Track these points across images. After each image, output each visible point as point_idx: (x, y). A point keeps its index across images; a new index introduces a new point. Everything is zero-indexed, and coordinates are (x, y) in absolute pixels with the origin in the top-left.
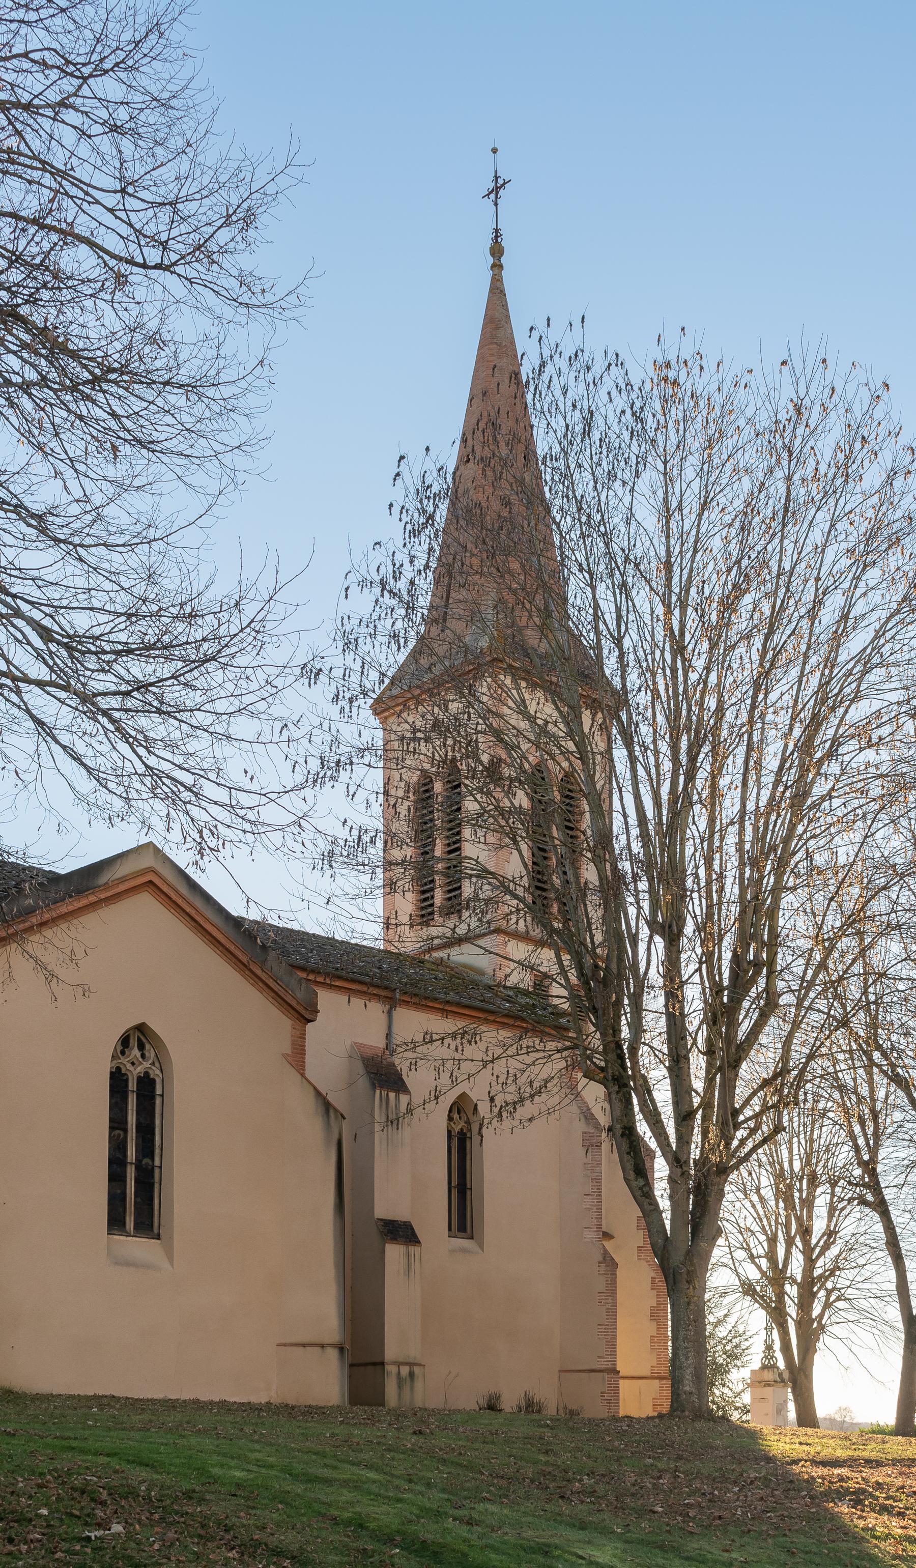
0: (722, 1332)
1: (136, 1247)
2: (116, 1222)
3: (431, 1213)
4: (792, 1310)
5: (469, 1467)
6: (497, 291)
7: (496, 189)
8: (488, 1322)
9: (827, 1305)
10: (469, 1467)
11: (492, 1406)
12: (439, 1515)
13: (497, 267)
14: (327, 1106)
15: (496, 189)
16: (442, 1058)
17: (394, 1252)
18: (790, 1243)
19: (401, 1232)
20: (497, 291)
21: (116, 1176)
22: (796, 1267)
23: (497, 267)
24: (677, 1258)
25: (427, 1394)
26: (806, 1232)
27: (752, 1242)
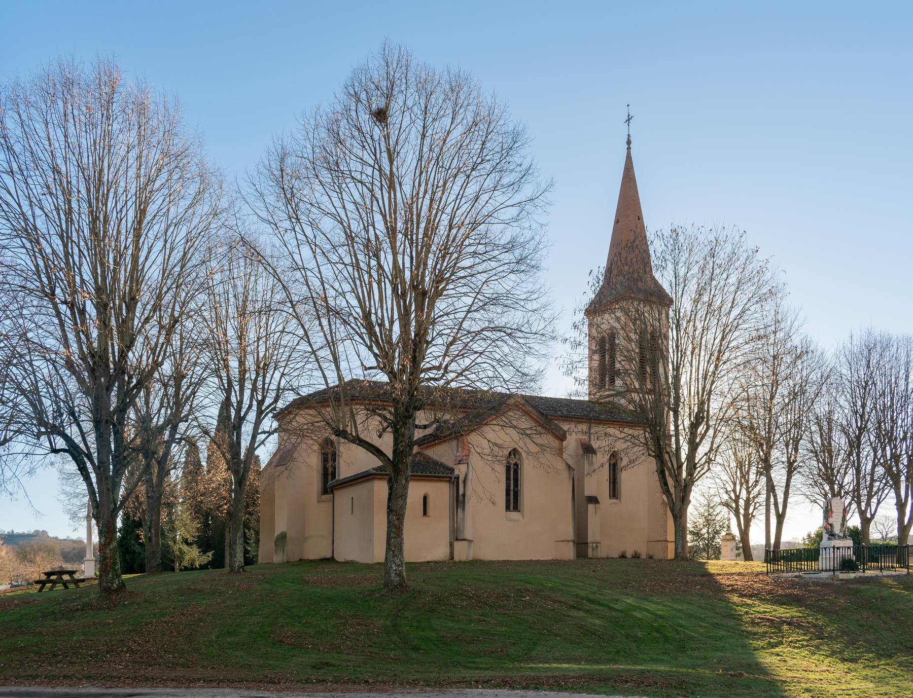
0: (718, 518)
1: (514, 515)
2: (508, 508)
3: (603, 492)
4: (742, 511)
5: (605, 581)
6: (629, 158)
7: (629, 120)
8: (628, 522)
9: (755, 509)
10: (605, 581)
11: (623, 556)
12: (595, 593)
13: (629, 148)
14: (569, 467)
15: (629, 120)
16: (609, 439)
17: (591, 507)
18: (741, 485)
19: (593, 500)
20: (629, 158)
21: (508, 494)
22: (744, 494)
23: (629, 148)
24: (677, 510)
25: (602, 552)
26: (747, 482)
27: (727, 486)
